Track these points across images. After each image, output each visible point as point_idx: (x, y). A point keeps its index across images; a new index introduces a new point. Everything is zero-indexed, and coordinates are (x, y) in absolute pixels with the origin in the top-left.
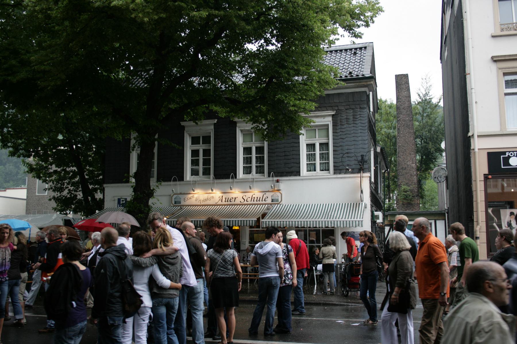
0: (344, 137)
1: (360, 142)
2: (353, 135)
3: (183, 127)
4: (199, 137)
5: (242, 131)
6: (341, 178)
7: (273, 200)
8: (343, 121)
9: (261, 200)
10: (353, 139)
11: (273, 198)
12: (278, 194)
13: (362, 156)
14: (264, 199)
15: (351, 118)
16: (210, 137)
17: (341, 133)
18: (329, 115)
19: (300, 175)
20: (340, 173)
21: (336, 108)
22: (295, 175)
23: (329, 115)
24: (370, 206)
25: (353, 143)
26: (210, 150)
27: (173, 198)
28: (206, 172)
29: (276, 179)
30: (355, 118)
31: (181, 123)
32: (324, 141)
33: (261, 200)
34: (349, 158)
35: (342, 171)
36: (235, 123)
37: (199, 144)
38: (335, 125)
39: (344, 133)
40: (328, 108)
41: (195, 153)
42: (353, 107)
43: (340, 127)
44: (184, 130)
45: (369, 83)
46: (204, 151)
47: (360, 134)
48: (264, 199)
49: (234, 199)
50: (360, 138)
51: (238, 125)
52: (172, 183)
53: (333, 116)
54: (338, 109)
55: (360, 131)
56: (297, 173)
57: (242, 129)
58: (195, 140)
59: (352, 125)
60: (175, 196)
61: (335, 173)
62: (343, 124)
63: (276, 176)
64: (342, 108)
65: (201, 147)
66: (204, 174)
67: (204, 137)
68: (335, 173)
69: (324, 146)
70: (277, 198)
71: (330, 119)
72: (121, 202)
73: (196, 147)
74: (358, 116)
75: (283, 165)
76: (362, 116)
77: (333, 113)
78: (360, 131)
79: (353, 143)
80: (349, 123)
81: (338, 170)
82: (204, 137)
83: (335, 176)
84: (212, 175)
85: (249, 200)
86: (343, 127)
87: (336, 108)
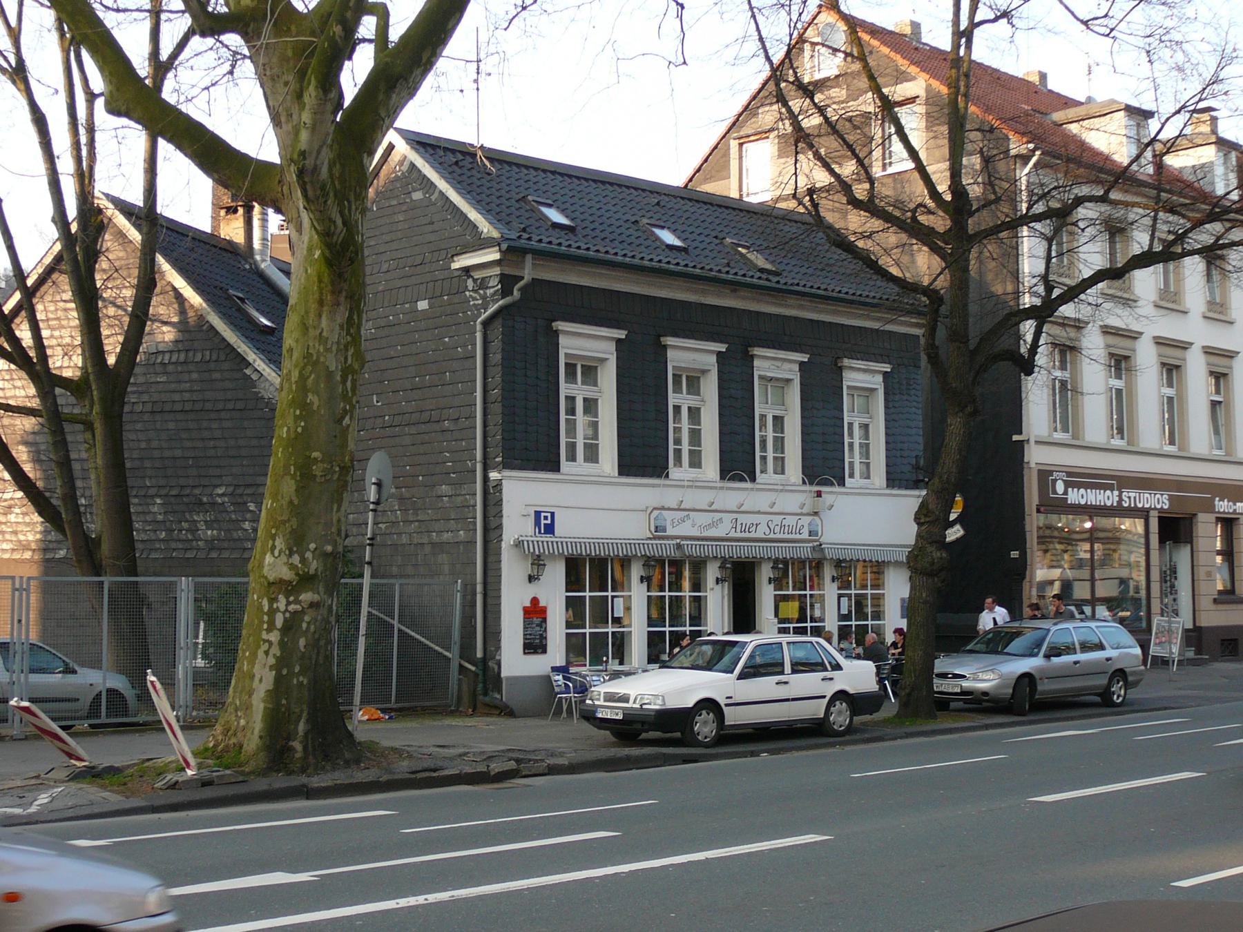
7: (810, 533)
12: (816, 518)
60: (656, 513)
83: (888, 491)
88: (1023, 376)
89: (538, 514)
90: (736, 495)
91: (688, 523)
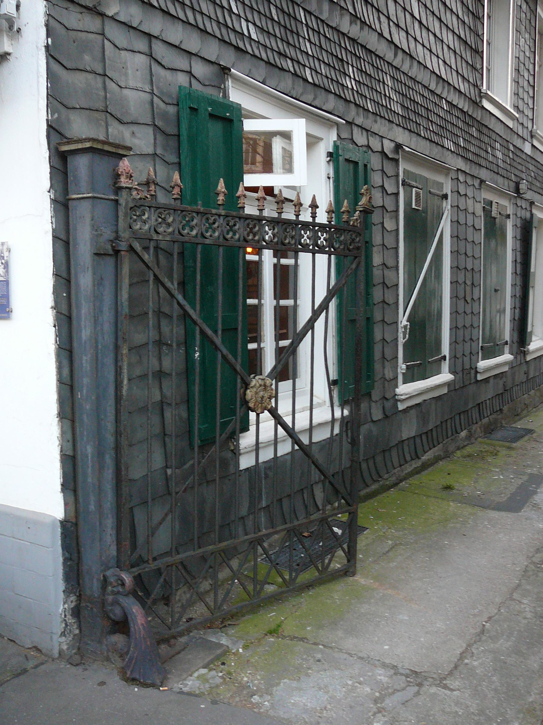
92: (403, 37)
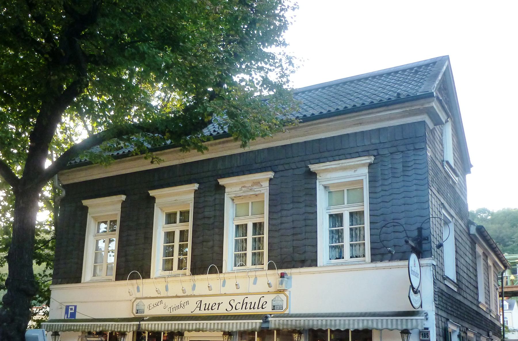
0: (387, 199)
1: (416, 206)
2: (403, 195)
3: (153, 199)
4: (175, 214)
5: (325, 187)
6: (384, 268)
7: (274, 308)
8: (386, 172)
9: (256, 306)
10: (402, 201)
11: (275, 303)
12: (282, 296)
13: (420, 230)
14: (260, 306)
15: (400, 166)
16: (188, 212)
17: (383, 193)
18: (363, 165)
19: (316, 265)
20: (381, 261)
21: (375, 153)
22: (310, 266)
23: (363, 165)
24: (434, 317)
25: (403, 208)
26: (363, 212)
27: (135, 304)
28: (257, 258)
29: (281, 271)
30: (405, 166)
31: (150, 192)
32: (355, 209)
33: (256, 306)
34: (397, 234)
35: (385, 256)
36: (313, 175)
37: (175, 222)
38: (372, 180)
39: (387, 193)
40: (361, 154)
41: (169, 236)
42: (402, 148)
43: (380, 183)
44: (316, 178)
45: (427, 106)
46: (255, 225)
47: (415, 193)
48: (260, 306)
49: (217, 305)
50: (415, 200)
51: (226, 190)
52: (127, 282)
53: (370, 165)
54: (378, 155)
55: (415, 187)
56: (313, 262)
57: (93, 215)
58: (171, 218)
59: (401, 179)
60: (138, 301)
61: (373, 261)
62: (386, 177)
63: (280, 268)
64: (386, 152)
65: (177, 228)
66: (180, 268)
67: (181, 213)
68: (373, 261)
69: (258, 227)
70: (280, 303)
71: (365, 171)
72: (70, 311)
73: (171, 228)
74: (410, 164)
75: (292, 250)
76: (417, 162)
77: (369, 161)
78: (415, 187)
79: (403, 208)
80: (396, 175)
81: (378, 255)
82: (181, 213)
83: (373, 265)
84: (188, 271)
85: (239, 306)
86: (386, 183)
87: (375, 153)
88: (196, 186)
89: (67, 308)
90: (205, 282)
91: (161, 306)
92: (181, 306)
